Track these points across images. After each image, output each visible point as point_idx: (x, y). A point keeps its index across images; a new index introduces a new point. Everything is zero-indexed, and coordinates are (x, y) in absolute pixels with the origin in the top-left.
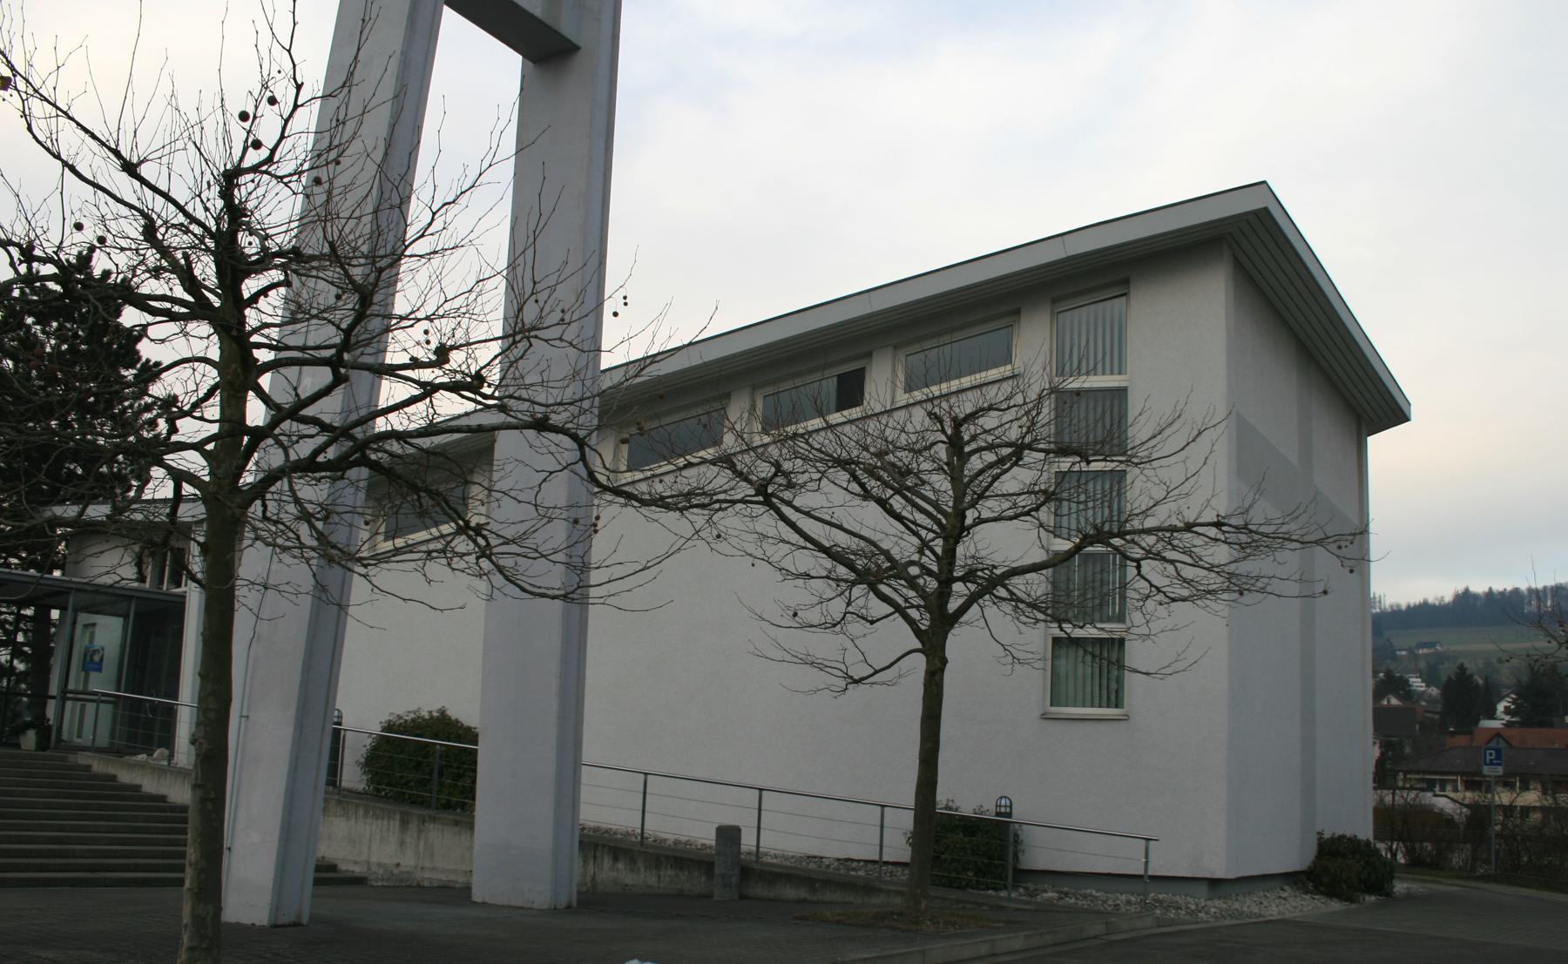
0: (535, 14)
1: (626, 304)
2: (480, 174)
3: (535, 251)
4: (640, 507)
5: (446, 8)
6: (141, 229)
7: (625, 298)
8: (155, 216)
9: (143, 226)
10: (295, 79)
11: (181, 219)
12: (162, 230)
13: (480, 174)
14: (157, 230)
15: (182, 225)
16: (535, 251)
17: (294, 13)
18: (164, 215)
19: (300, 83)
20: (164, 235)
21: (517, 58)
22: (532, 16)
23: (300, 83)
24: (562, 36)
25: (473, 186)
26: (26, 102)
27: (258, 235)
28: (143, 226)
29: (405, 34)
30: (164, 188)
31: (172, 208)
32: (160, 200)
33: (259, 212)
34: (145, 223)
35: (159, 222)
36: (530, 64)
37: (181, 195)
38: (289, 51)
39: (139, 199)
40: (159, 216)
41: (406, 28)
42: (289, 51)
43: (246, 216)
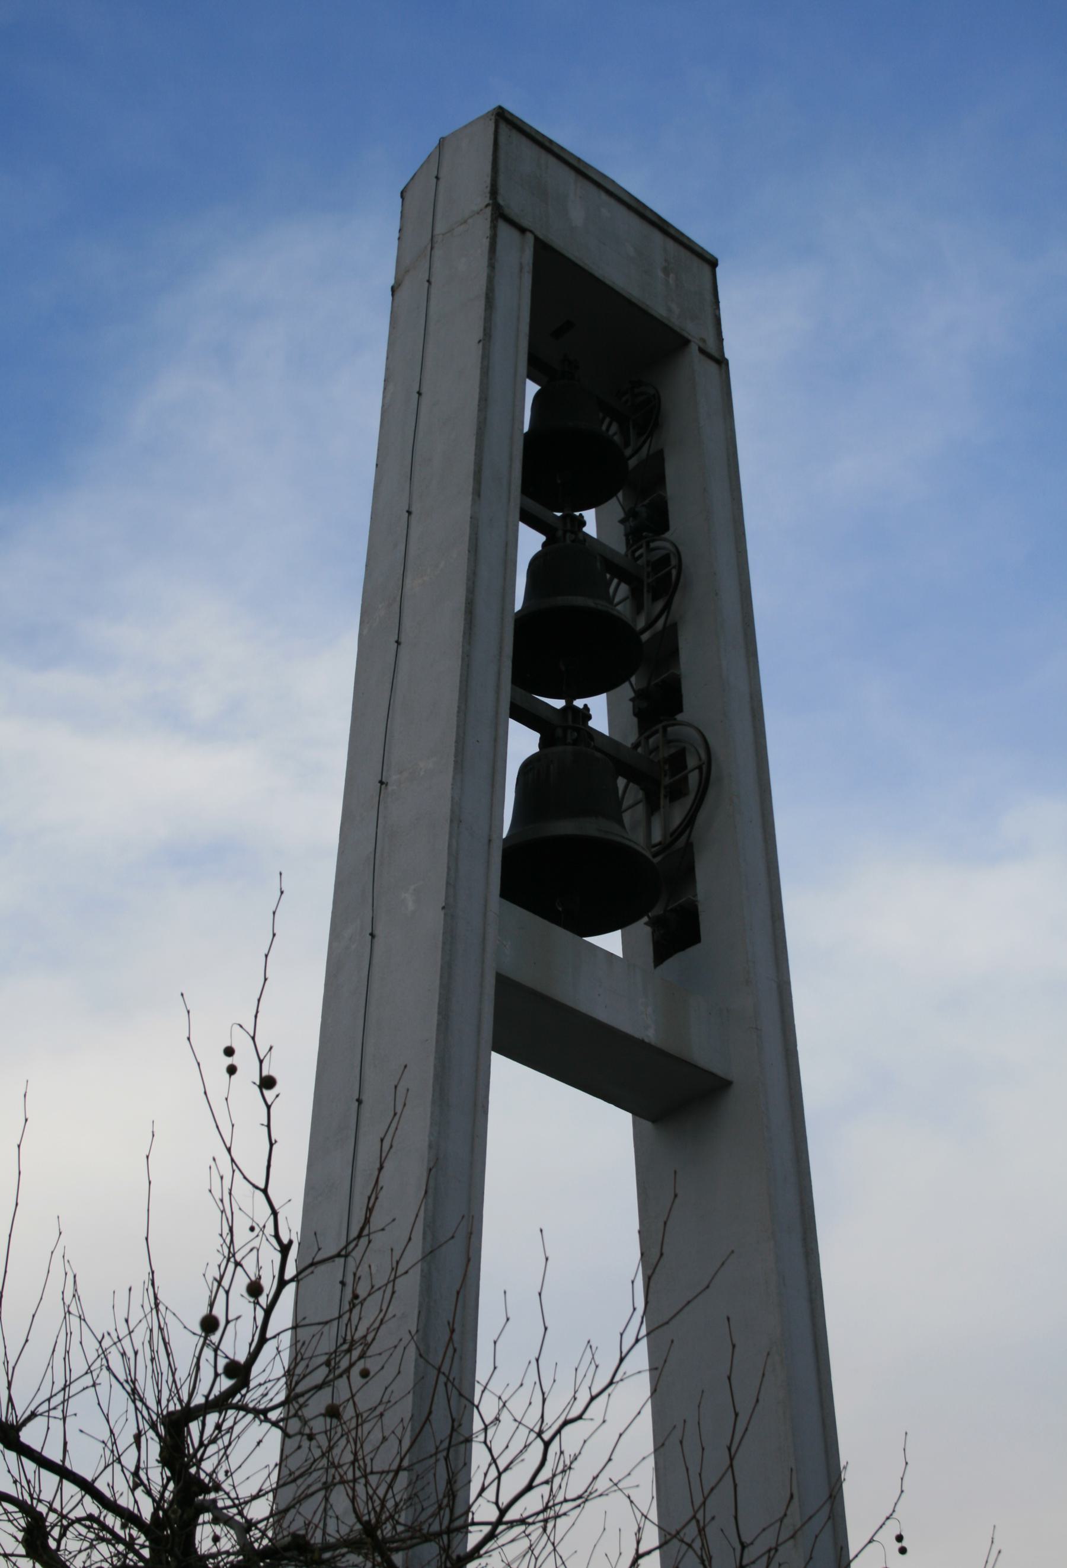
0: (646, 1040)
1: (903, 1551)
2: (622, 1360)
3: (735, 1486)
4: (248, 1387)
5: (496, 1058)
6: (20, 1535)
7: (900, 1538)
8: (42, 1509)
9: (24, 1530)
10: (277, 1236)
11: (91, 1506)
12: (56, 1532)
13: (622, 1360)
14: (49, 1533)
15: (90, 1517)
16: (735, 1486)
17: (269, 1126)
18: (57, 1505)
19: (285, 1241)
20: (59, 1542)
21: (625, 1118)
22: (641, 1044)
23: (285, 1241)
24: (696, 1066)
25: (611, 1383)
26: (86, 1539)
27: (228, 1522)
28: (24, 1530)
29: (432, 1113)
30: (56, 1456)
31: (69, 1488)
32: (50, 1479)
33: (230, 1481)
34: (28, 1523)
35: (52, 1518)
36: (648, 1125)
37: (83, 1465)
38: (265, 1191)
39: (15, 1482)
40: (51, 1509)
41: (433, 1102)
42: (265, 1191)
43: (206, 1490)
